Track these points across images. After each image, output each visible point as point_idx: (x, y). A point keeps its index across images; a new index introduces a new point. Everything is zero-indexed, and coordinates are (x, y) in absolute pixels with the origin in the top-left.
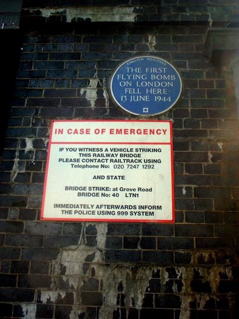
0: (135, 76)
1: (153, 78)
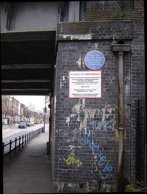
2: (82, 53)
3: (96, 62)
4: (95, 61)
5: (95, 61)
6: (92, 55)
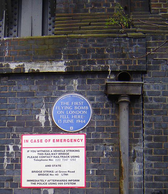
0: (68, 120)
1: (76, 108)
2: (47, 99)
3: (75, 117)
4: (74, 114)
5: (74, 114)
6: (67, 103)
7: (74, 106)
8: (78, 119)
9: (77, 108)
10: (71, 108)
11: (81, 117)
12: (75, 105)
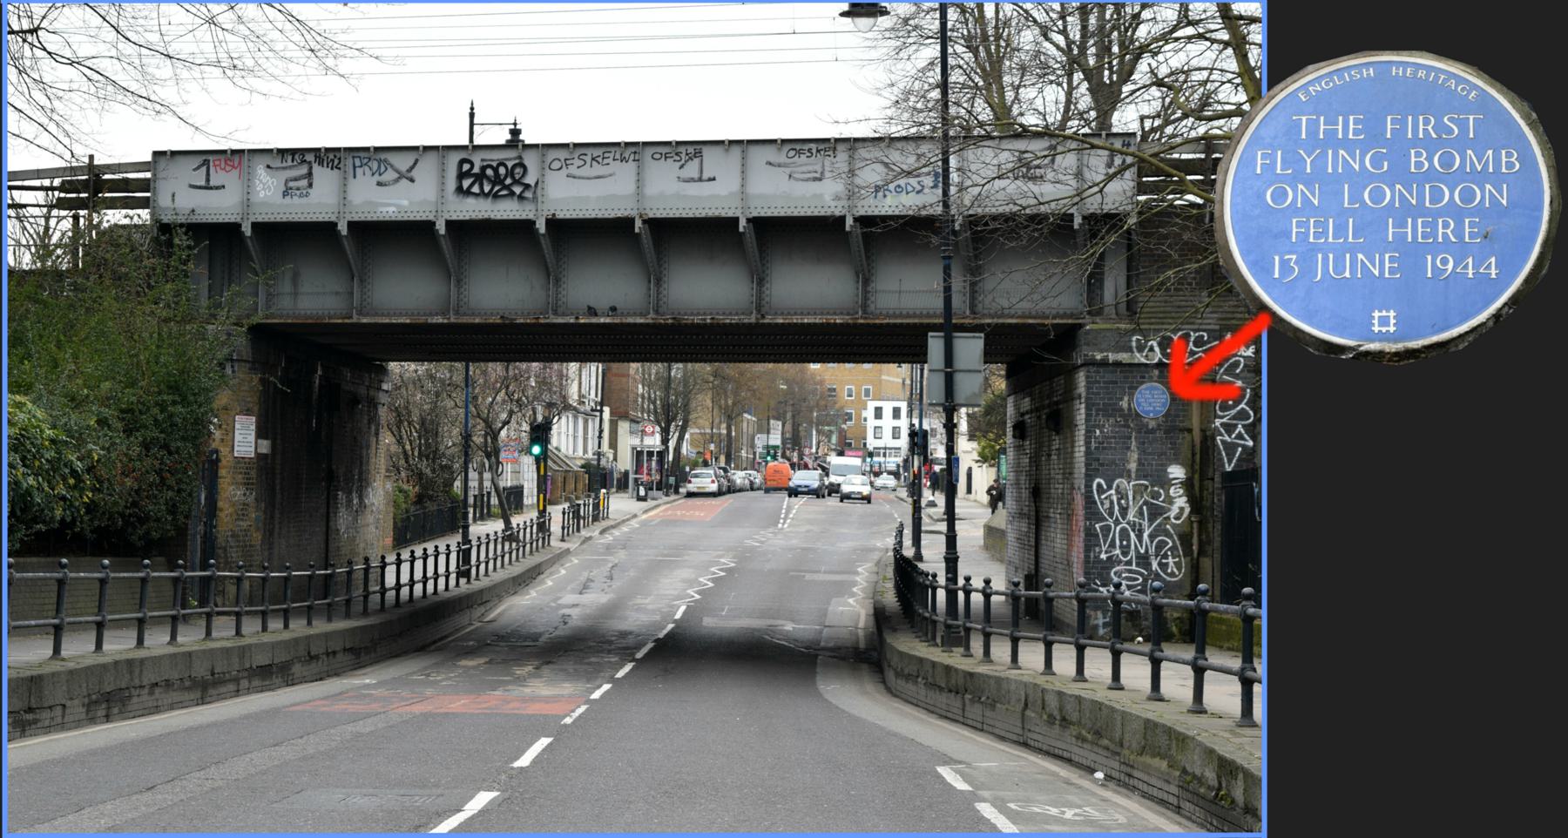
2: (1129, 388)
3: (1414, 230)
4: (1406, 211)
5: (1406, 211)
6: (1348, 127)
7: (1399, 147)
8: (1435, 248)
9: (1430, 159)
10: (1376, 162)
11: (1459, 232)
12: (1415, 142)
